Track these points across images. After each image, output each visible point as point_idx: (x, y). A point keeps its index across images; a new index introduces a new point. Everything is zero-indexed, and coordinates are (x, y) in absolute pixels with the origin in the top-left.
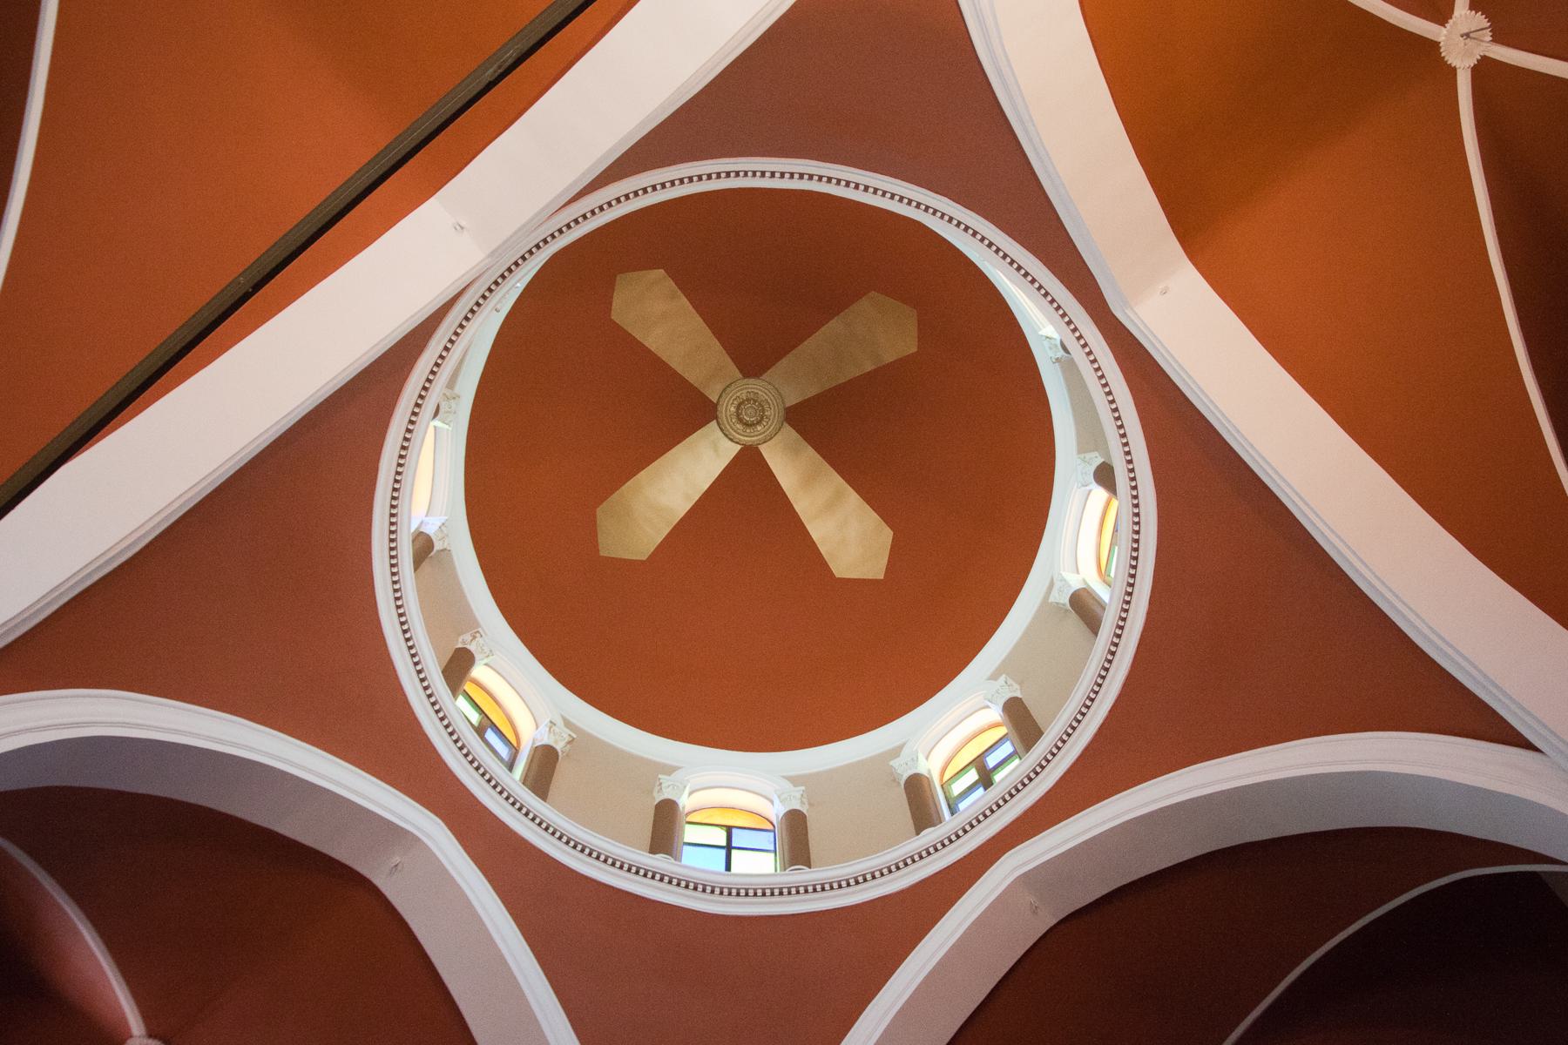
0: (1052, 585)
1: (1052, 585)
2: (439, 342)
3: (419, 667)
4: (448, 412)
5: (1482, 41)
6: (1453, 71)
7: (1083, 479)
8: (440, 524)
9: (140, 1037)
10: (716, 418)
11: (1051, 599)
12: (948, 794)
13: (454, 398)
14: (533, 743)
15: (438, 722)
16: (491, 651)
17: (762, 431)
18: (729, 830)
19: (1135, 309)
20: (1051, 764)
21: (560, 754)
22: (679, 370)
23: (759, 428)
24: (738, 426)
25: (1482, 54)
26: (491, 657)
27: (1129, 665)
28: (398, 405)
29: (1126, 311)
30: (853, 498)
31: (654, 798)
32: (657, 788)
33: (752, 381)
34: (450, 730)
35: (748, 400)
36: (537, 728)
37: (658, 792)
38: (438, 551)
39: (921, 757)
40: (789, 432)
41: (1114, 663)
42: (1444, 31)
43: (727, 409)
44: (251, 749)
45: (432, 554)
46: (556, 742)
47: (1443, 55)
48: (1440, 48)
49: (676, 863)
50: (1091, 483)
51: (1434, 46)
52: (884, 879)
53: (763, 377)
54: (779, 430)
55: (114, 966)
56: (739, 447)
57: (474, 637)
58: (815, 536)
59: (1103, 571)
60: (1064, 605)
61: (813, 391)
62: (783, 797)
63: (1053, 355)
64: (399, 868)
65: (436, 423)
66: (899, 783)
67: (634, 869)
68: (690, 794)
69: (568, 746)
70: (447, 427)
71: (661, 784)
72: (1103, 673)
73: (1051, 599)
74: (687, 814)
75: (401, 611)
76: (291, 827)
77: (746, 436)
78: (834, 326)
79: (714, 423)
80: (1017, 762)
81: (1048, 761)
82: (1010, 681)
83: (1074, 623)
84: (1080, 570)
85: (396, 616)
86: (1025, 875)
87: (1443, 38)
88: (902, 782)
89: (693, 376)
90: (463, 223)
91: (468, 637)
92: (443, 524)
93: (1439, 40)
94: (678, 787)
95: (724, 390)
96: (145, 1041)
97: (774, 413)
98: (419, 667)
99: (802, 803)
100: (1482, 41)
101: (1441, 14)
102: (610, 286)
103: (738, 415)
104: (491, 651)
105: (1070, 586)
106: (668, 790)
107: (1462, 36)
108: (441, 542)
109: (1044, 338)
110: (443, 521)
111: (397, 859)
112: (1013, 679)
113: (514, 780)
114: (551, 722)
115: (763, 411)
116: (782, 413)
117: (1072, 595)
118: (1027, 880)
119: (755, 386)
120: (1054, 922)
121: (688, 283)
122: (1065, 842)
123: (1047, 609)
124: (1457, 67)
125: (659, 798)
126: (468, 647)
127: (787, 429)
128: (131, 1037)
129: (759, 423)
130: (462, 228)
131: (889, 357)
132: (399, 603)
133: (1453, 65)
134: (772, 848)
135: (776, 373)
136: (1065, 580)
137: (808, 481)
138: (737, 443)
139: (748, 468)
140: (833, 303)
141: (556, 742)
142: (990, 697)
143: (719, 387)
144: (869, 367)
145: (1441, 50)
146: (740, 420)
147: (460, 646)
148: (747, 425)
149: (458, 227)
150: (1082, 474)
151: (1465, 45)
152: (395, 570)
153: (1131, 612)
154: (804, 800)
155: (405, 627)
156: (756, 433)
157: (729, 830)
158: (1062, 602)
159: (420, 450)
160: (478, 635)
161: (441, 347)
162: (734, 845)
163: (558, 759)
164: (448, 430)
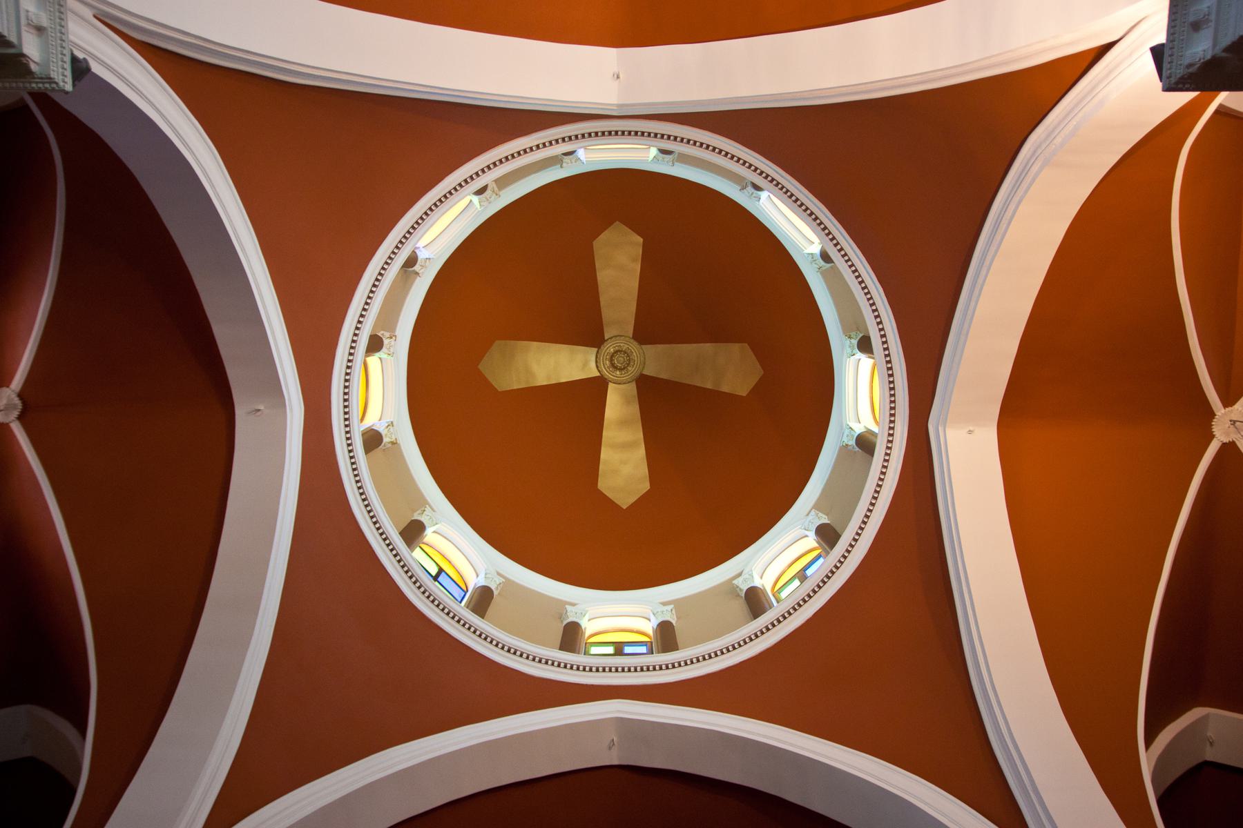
0: (740, 575)
1: (740, 575)
2: (538, 139)
3: (364, 313)
4: (486, 198)
5: (1239, 432)
6: (1212, 436)
7: (809, 525)
8: (428, 257)
9: (13, 391)
10: (599, 347)
11: (735, 582)
12: (587, 649)
13: (497, 195)
14: (372, 426)
15: (347, 353)
16: (393, 353)
17: (619, 376)
18: (441, 570)
19: (947, 429)
20: (680, 669)
21: (383, 444)
22: (602, 303)
23: (618, 373)
24: (607, 362)
25: (1234, 439)
26: (389, 357)
27: (775, 642)
28: (488, 152)
29: (940, 428)
30: (641, 452)
31: (413, 516)
32: (419, 512)
33: (635, 343)
34: (350, 364)
35: (625, 352)
36: (380, 420)
37: (419, 514)
38: (414, 271)
39: (587, 617)
40: (632, 388)
41: (765, 636)
42: (1223, 411)
43: (609, 348)
44: (248, 261)
45: (411, 269)
46: (386, 435)
47: (1213, 423)
48: (1214, 418)
49: (1213, 17)
50: (657, 618)
51: (1211, 414)
52: (526, 661)
53: (643, 346)
54: (629, 382)
55: (41, 333)
56: (598, 374)
57: (391, 338)
58: (603, 456)
59: (776, 590)
60: (741, 590)
61: (664, 376)
62: (488, 576)
63: (846, 441)
64: (259, 413)
65: (475, 199)
66: (562, 622)
67: (384, 536)
68: (434, 532)
69: (390, 445)
70: (478, 206)
71: (424, 511)
72: (753, 637)
73: (735, 582)
74: (423, 543)
75: (383, 272)
76: (222, 333)
77: (607, 371)
78: (708, 347)
79: (596, 349)
80: (821, 560)
81: (680, 665)
82: (674, 612)
83: (740, 607)
84: (763, 577)
85: (377, 272)
86: (622, 719)
87: (1220, 414)
88: (565, 623)
89: (607, 314)
90: (621, 76)
91: (387, 334)
92: (429, 259)
93: (1217, 413)
94: (433, 521)
95: (616, 336)
96: (14, 396)
97: (633, 371)
98: (364, 313)
99: (497, 588)
100: (1239, 432)
101: (1228, 401)
102: (607, 224)
103: (612, 356)
104: (393, 353)
105: (753, 581)
106: (426, 517)
107: (1231, 421)
108: (420, 268)
109: (848, 427)
110: (431, 257)
111: (261, 407)
112: (676, 612)
113: (357, 431)
114: (392, 423)
115: (628, 365)
116: (638, 374)
117: (752, 587)
118: (623, 724)
119: (634, 347)
120: (616, 762)
121: (649, 259)
122: (665, 717)
123: (729, 588)
124: (1216, 436)
125: (416, 517)
126: (384, 339)
127: (633, 385)
128: (8, 387)
129: (621, 369)
130: (618, 77)
131: (725, 388)
132: (386, 266)
133: (1214, 433)
134: (459, 600)
135: (650, 350)
136: (753, 577)
137: (623, 423)
138: (599, 371)
139: (594, 390)
140: (717, 334)
141: (386, 435)
142: (655, 612)
143: (615, 333)
144: (709, 386)
145: (1214, 420)
146: (611, 360)
147: (379, 334)
148: (613, 365)
149: (616, 76)
150: (810, 522)
151: (1229, 427)
152: (400, 246)
153: (781, 624)
154: (499, 588)
155: (377, 283)
156: (614, 374)
157: (441, 570)
158: (742, 587)
159: (427, 230)
160: (394, 338)
161: (536, 143)
162: (439, 579)
163: (380, 445)
164: (477, 208)
